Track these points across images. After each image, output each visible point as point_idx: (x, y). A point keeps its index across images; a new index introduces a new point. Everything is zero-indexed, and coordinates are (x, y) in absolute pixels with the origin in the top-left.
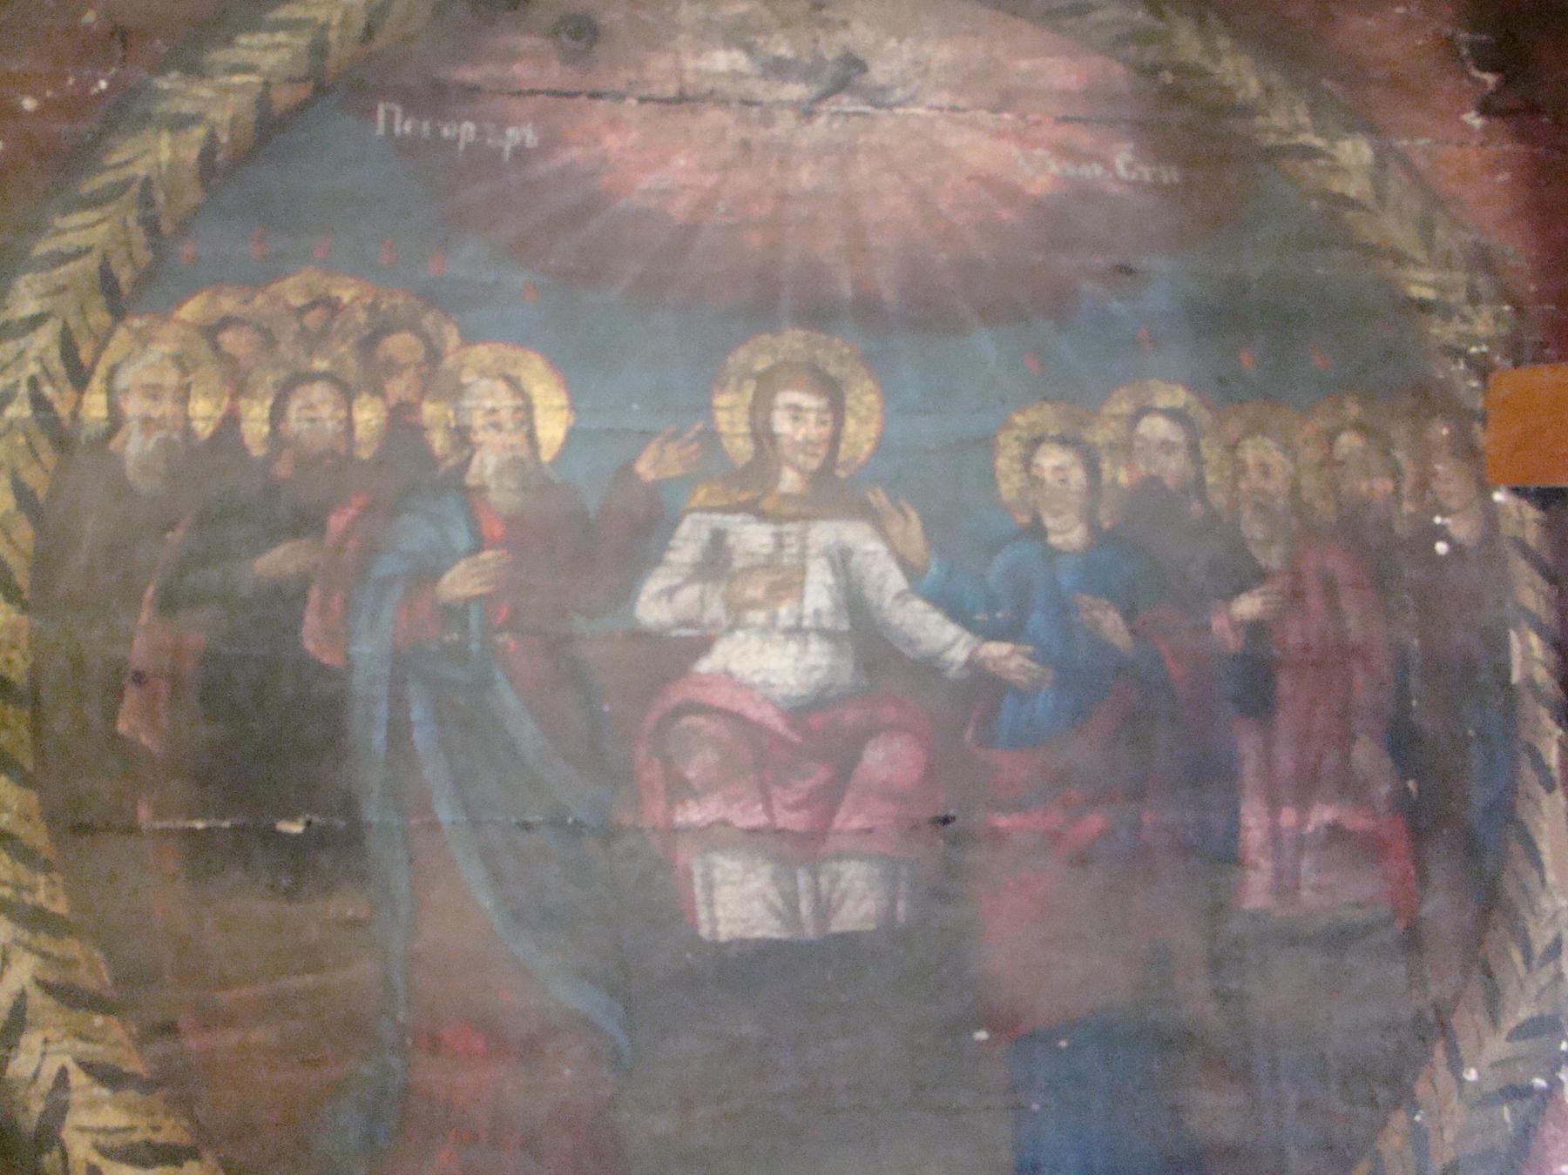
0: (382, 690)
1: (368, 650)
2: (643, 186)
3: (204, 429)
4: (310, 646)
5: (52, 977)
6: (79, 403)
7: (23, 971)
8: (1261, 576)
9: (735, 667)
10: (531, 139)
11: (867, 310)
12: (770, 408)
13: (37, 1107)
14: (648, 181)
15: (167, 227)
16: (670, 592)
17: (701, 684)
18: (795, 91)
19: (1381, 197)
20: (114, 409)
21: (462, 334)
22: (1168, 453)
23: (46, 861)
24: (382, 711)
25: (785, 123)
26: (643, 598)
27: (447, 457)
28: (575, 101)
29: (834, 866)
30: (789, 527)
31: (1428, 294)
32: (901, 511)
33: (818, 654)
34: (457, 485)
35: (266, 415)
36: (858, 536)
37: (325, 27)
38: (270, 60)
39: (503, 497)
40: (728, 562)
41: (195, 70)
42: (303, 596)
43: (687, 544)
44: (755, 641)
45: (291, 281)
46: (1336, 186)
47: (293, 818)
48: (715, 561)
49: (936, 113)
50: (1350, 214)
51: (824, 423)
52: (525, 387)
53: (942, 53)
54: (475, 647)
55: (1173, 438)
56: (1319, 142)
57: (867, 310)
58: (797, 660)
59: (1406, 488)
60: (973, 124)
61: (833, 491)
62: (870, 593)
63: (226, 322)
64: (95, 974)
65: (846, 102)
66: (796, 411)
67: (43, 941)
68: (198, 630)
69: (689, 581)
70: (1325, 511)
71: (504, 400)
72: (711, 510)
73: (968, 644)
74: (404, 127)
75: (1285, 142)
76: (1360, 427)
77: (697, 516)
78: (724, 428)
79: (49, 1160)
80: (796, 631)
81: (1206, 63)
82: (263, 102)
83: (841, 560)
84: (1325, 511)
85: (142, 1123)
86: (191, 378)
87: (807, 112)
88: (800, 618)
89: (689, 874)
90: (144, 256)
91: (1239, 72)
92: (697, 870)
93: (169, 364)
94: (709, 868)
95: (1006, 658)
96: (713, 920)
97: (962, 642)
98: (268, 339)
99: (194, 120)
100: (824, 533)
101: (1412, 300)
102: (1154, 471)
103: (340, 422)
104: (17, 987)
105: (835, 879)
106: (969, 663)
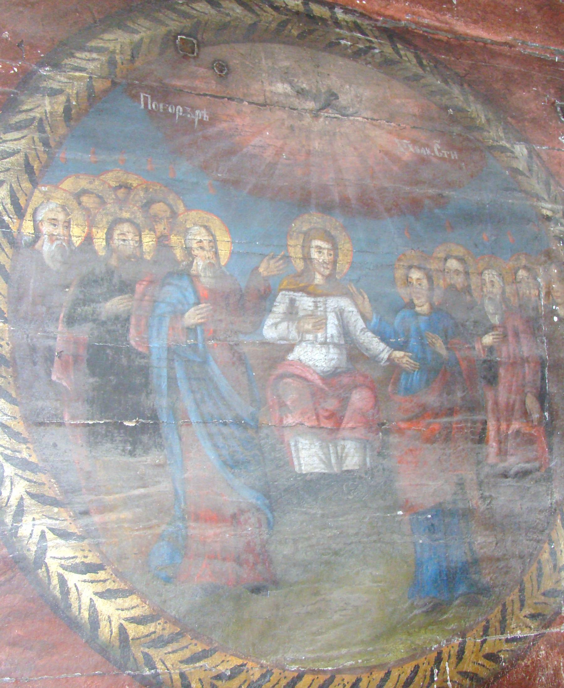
0: (164, 364)
1: (158, 344)
2: (253, 143)
3: (77, 241)
4: (133, 343)
5: (33, 490)
6: (21, 225)
7: (20, 488)
8: (493, 328)
9: (302, 358)
10: (206, 118)
11: (345, 205)
12: (310, 247)
13: (34, 548)
14: (256, 141)
15: (52, 144)
16: (276, 325)
17: (290, 365)
18: (310, 105)
19: (530, 170)
20: (36, 229)
21: (185, 206)
22: (458, 275)
23: (24, 438)
24: (164, 372)
25: (308, 119)
26: (265, 327)
27: (183, 261)
28: (222, 100)
29: (342, 442)
30: (319, 299)
31: (549, 213)
32: (360, 293)
33: (333, 353)
34: (185, 273)
35: (104, 237)
36: (345, 303)
37: (114, 52)
38: (91, 66)
39: (206, 280)
40: (297, 313)
41: (57, 66)
42: (128, 320)
43: (280, 306)
44: (309, 348)
45: (110, 174)
46: (515, 164)
47: (131, 420)
48: (292, 312)
49: (366, 120)
50: (520, 177)
51: (331, 255)
52: (213, 231)
53: (367, 93)
54: (200, 346)
55: (459, 269)
56: (508, 145)
57: (345, 205)
58: (325, 356)
59: (542, 295)
60: (380, 127)
61: (335, 286)
62: (351, 328)
63: (85, 192)
64: (53, 491)
65: (331, 112)
66: (320, 249)
67: (28, 474)
68: (84, 332)
69: (283, 320)
70: (515, 302)
71: (203, 236)
72: (289, 290)
73: (388, 351)
74: (152, 105)
75: (495, 144)
76: (525, 267)
77: (284, 292)
78: (292, 254)
79: (41, 572)
80: (324, 343)
81: (465, 106)
82: (90, 87)
83: (340, 314)
84: (515, 302)
85: (79, 554)
86: (70, 217)
87: (316, 116)
88: (326, 338)
89: (289, 445)
90: (44, 157)
91: (477, 111)
92: (292, 444)
93: (60, 209)
94: (296, 443)
95: (403, 357)
96: (300, 465)
97: (386, 350)
98: (102, 202)
99: (60, 92)
100: (333, 302)
101: (543, 215)
102: (452, 282)
103: (136, 242)
104: (18, 496)
105: (344, 448)
106: (389, 359)
